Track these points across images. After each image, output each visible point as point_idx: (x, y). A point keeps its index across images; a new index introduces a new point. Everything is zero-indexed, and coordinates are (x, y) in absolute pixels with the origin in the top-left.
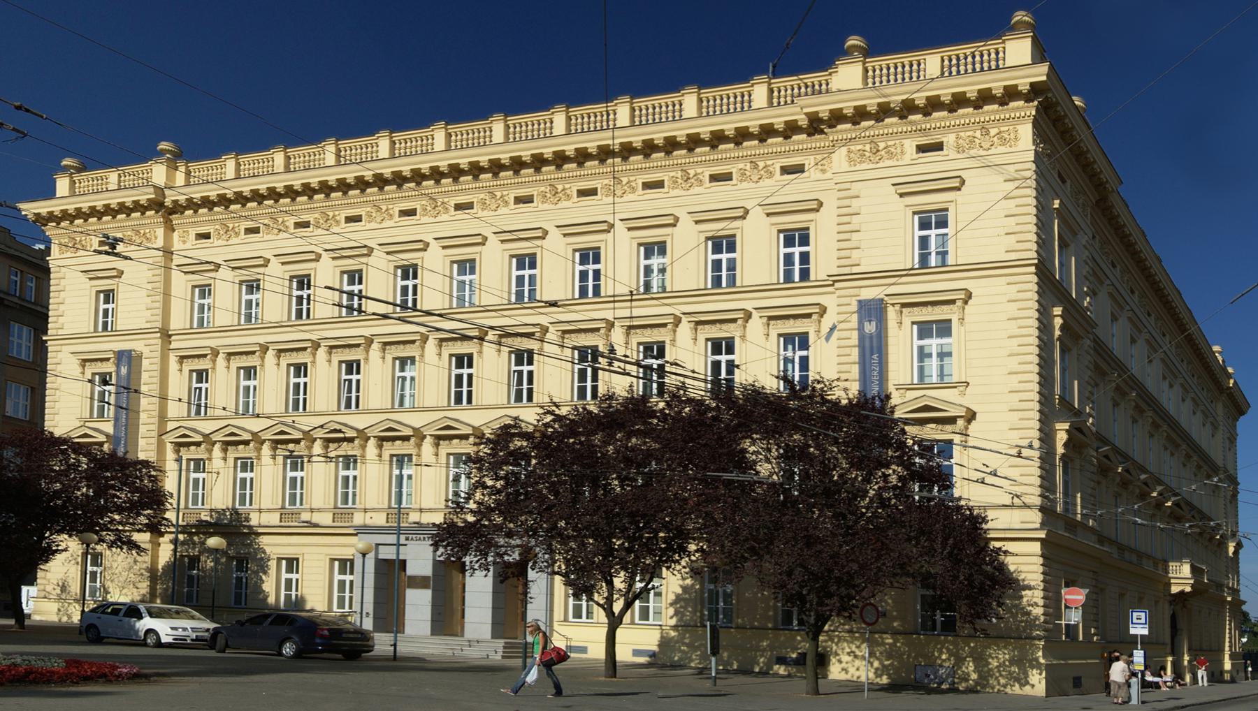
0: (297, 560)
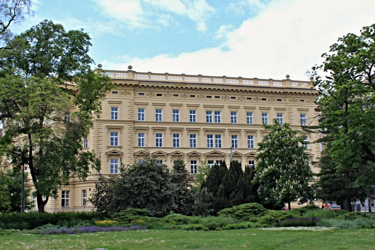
0: (86, 190)
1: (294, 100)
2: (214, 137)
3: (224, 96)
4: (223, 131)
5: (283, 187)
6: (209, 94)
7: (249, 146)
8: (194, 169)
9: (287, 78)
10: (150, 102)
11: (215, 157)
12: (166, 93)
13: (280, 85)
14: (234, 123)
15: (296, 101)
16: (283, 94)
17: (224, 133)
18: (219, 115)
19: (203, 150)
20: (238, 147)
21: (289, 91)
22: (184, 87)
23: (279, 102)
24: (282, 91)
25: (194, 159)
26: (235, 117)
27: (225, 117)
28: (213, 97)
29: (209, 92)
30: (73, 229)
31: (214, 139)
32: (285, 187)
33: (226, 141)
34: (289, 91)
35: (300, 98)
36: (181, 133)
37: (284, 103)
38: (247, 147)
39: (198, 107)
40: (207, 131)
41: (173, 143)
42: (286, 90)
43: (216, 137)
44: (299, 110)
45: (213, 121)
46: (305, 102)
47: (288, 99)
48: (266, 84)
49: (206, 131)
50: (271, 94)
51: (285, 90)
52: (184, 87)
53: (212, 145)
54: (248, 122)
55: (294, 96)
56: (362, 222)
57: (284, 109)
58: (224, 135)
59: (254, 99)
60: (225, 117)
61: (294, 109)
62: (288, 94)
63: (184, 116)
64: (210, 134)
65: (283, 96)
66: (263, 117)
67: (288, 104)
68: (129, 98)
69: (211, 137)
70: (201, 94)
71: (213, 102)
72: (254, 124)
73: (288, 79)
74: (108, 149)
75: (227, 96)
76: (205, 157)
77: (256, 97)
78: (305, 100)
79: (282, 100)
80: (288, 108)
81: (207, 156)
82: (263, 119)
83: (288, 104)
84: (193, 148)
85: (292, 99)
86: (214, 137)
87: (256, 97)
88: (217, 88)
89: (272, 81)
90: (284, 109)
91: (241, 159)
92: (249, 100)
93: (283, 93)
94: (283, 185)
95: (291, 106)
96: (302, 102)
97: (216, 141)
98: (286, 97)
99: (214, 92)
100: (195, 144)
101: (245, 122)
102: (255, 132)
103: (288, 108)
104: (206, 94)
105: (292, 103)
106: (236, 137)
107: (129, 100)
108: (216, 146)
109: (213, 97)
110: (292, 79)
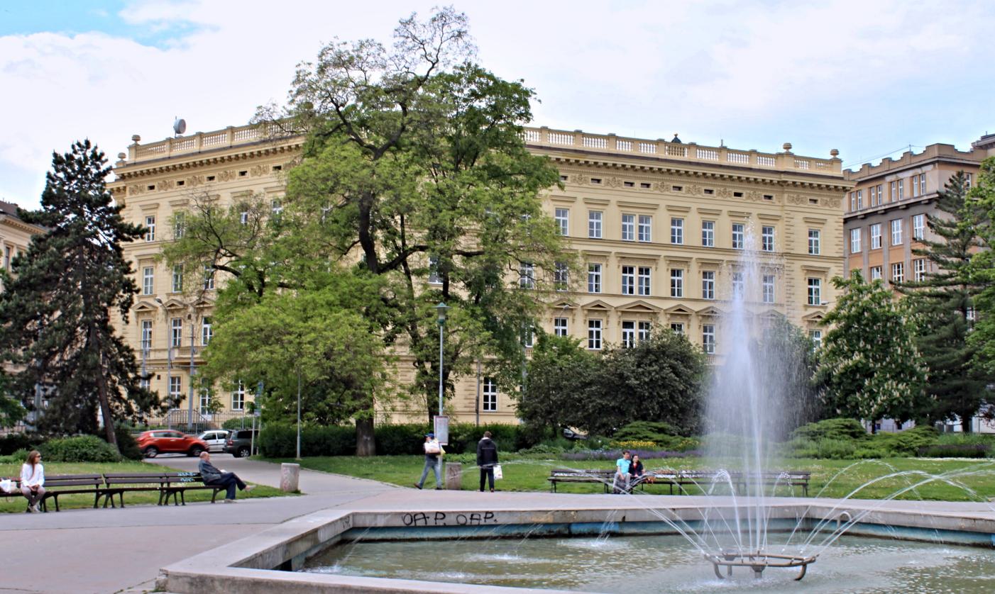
1: (799, 200)
2: (636, 271)
3: (660, 183)
4: (654, 259)
5: (878, 393)
6: (630, 177)
7: (705, 295)
8: (595, 339)
9: (785, 151)
10: (725, 209)
11: (638, 315)
12: (828, 199)
13: (771, 165)
14: (676, 243)
15: (802, 202)
16: (778, 186)
17: (657, 264)
18: (564, 218)
19: (616, 298)
20: (683, 296)
21: (790, 179)
22: (582, 161)
23: (767, 201)
24: (776, 178)
25: (595, 317)
26: (597, 223)
27: (660, 229)
28: (637, 184)
29: (630, 174)
30: (597, 452)
31: (636, 275)
32: (884, 395)
33: (660, 280)
34: (790, 179)
35: (707, 185)
36: (823, 278)
37: (777, 203)
38: (701, 297)
39: (823, 224)
40: (624, 258)
41: (669, 288)
42: (784, 178)
43: (641, 271)
44: (807, 221)
45: (636, 238)
46: (819, 203)
47: (786, 195)
48: (602, 146)
49: (623, 257)
50: (622, 170)
51: (783, 176)
52: (582, 161)
53: (631, 290)
54: (704, 242)
55: (800, 190)
56: (423, 474)
57: (776, 218)
58: (656, 269)
59: (719, 194)
60: (660, 229)
61: (798, 219)
62: (788, 185)
63: (692, 232)
64: (628, 264)
65: (778, 188)
66: (592, 220)
67: (786, 208)
68: (835, 213)
69: (631, 270)
70: (755, 190)
71: (637, 195)
72: (717, 247)
73: (787, 154)
74: (806, 310)
75: (757, 193)
76: (620, 314)
77: (722, 189)
78: (819, 199)
79: (774, 198)
80: (786, 215)
81: (623, 312)
82: (591, 225)
83: (786, 208)
84: (814, 307)
85: (795, 196)
86: (636, 271)
87: (722, 189)
88: (619, 163)
89: (726, 152)
90: (776, 218)
91: (575, 315)
92: (708, 196)
93: (779, 182)
94: (879, 390)
95: (792, 213)
96: (812, 205)
97: (641, 279)
98: (783, 192)
99: (640, 174)
100: (771, 296)
101: (618, 237)
102: (604, 256)
103: (786, 215)
104: (764, 191)
105: (793, 204)
106: (816, 282)
107: (836, 217)
108: (640, 290)
109: (637, 184)
110: (796, 154)
